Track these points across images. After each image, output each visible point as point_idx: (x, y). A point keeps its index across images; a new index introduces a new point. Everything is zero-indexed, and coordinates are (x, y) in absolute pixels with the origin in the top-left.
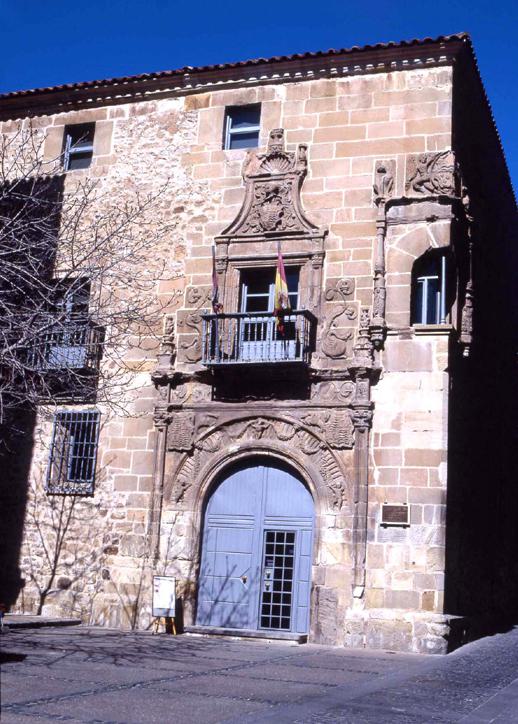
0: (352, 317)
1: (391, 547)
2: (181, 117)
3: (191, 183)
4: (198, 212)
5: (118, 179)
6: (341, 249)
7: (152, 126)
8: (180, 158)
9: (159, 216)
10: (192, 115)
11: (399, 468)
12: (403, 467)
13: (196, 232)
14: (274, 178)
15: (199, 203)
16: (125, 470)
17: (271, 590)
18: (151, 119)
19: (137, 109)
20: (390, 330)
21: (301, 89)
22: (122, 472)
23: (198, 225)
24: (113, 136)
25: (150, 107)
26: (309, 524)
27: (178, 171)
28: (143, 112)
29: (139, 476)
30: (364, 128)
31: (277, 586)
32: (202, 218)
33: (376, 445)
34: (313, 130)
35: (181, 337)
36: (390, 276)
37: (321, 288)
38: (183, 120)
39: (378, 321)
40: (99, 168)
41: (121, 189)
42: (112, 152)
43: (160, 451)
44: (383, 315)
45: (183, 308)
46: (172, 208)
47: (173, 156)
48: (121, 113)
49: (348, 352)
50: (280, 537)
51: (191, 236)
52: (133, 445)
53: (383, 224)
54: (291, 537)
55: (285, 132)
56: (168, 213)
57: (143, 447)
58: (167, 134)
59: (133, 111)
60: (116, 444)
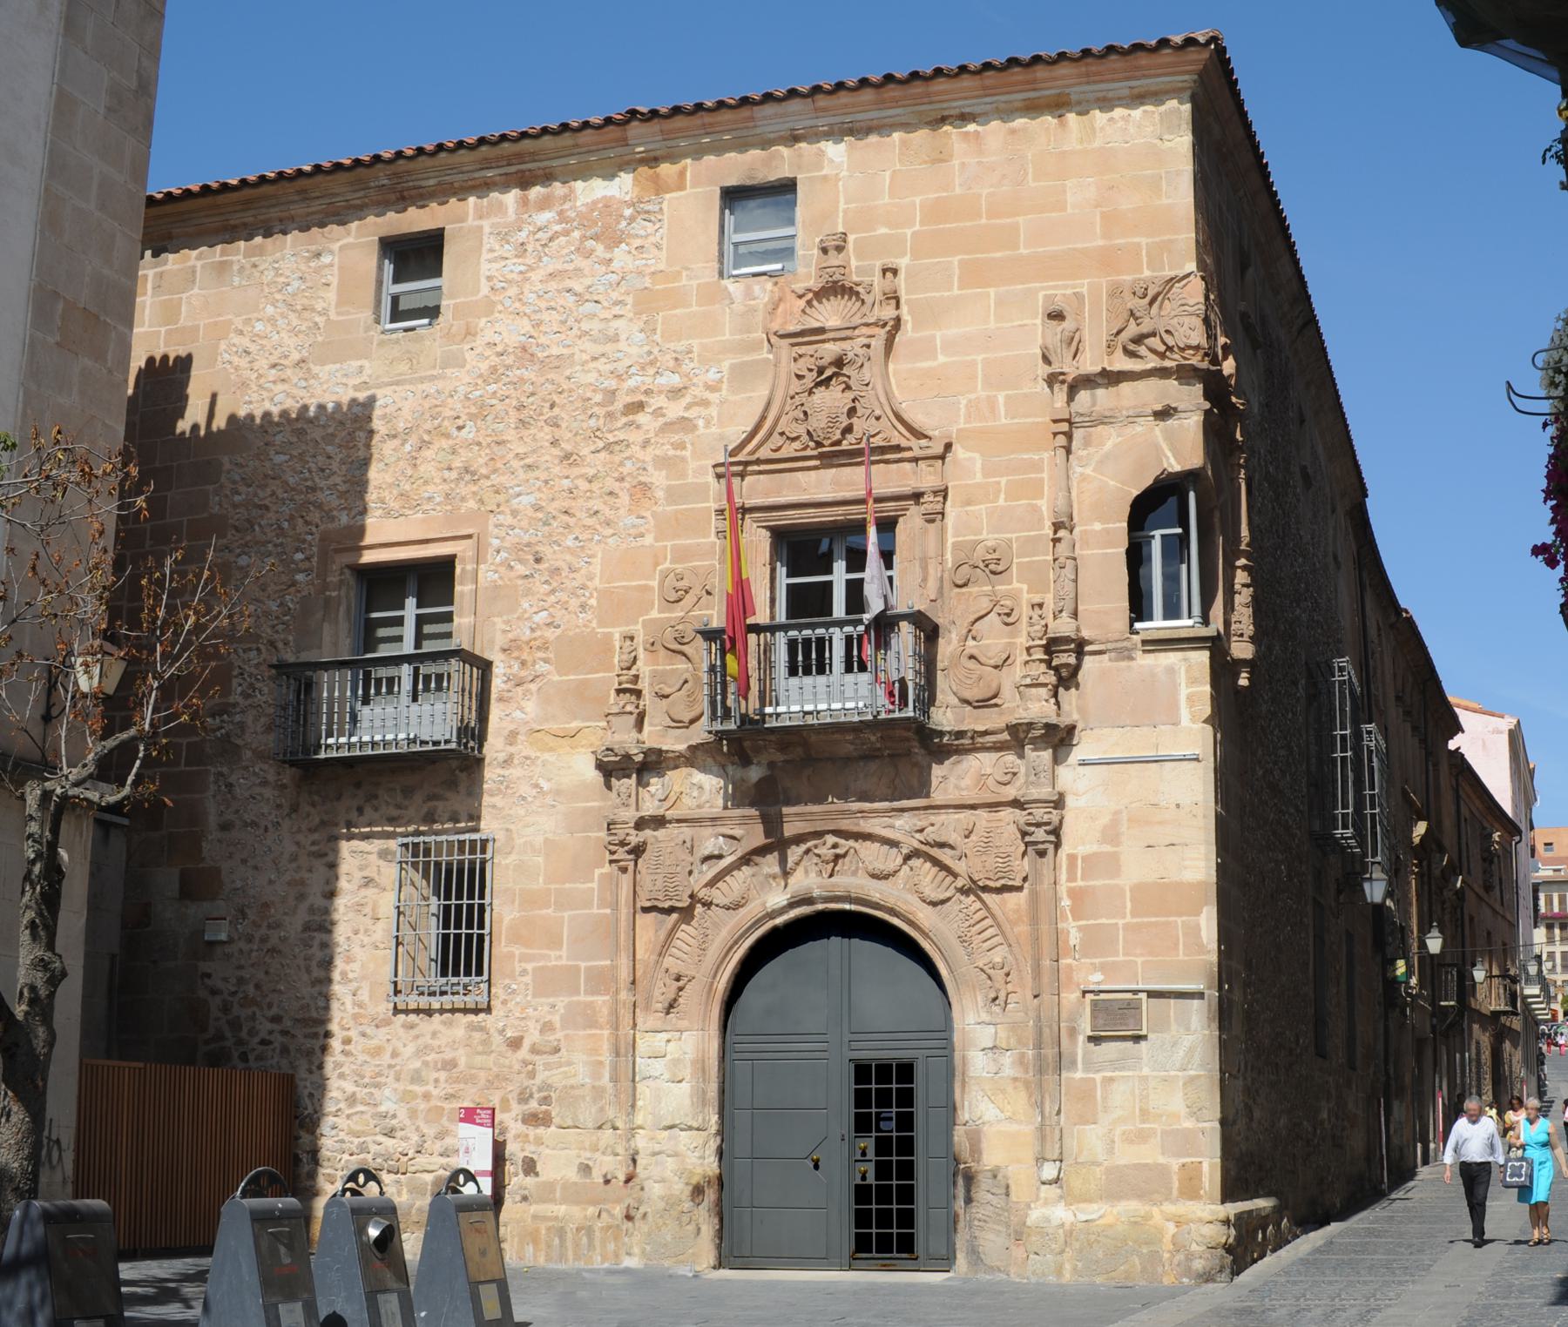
2: (628, 212)
4: (675, 410)
5: (499, 349)
6: (979, 478)
8: (630, 300)
9: (592, 422)
11: (1121, 922)
12: (1129, 919)
13: (671, 453)
15: (675, 393)
16: (552, 953)
17: (871, 1179)
18: (562, 218)
20: (1091, 643)
23: (676, 438)
24: (485, 256)
28: (544, 204)
29: (583, 965)
31: (882, 1170)
32: (685, 424)
34: (909, 232)
38: (632, 219)
41: (508, 367)
43: (625, 912)
45: (654, 614)
46: (618, 406)
47: (615, 295)
50: (884, 1070)
51: (663, 462)
56: (610, 415)
57: (587, 904)
58: (600, 249)
60: (531, 900)
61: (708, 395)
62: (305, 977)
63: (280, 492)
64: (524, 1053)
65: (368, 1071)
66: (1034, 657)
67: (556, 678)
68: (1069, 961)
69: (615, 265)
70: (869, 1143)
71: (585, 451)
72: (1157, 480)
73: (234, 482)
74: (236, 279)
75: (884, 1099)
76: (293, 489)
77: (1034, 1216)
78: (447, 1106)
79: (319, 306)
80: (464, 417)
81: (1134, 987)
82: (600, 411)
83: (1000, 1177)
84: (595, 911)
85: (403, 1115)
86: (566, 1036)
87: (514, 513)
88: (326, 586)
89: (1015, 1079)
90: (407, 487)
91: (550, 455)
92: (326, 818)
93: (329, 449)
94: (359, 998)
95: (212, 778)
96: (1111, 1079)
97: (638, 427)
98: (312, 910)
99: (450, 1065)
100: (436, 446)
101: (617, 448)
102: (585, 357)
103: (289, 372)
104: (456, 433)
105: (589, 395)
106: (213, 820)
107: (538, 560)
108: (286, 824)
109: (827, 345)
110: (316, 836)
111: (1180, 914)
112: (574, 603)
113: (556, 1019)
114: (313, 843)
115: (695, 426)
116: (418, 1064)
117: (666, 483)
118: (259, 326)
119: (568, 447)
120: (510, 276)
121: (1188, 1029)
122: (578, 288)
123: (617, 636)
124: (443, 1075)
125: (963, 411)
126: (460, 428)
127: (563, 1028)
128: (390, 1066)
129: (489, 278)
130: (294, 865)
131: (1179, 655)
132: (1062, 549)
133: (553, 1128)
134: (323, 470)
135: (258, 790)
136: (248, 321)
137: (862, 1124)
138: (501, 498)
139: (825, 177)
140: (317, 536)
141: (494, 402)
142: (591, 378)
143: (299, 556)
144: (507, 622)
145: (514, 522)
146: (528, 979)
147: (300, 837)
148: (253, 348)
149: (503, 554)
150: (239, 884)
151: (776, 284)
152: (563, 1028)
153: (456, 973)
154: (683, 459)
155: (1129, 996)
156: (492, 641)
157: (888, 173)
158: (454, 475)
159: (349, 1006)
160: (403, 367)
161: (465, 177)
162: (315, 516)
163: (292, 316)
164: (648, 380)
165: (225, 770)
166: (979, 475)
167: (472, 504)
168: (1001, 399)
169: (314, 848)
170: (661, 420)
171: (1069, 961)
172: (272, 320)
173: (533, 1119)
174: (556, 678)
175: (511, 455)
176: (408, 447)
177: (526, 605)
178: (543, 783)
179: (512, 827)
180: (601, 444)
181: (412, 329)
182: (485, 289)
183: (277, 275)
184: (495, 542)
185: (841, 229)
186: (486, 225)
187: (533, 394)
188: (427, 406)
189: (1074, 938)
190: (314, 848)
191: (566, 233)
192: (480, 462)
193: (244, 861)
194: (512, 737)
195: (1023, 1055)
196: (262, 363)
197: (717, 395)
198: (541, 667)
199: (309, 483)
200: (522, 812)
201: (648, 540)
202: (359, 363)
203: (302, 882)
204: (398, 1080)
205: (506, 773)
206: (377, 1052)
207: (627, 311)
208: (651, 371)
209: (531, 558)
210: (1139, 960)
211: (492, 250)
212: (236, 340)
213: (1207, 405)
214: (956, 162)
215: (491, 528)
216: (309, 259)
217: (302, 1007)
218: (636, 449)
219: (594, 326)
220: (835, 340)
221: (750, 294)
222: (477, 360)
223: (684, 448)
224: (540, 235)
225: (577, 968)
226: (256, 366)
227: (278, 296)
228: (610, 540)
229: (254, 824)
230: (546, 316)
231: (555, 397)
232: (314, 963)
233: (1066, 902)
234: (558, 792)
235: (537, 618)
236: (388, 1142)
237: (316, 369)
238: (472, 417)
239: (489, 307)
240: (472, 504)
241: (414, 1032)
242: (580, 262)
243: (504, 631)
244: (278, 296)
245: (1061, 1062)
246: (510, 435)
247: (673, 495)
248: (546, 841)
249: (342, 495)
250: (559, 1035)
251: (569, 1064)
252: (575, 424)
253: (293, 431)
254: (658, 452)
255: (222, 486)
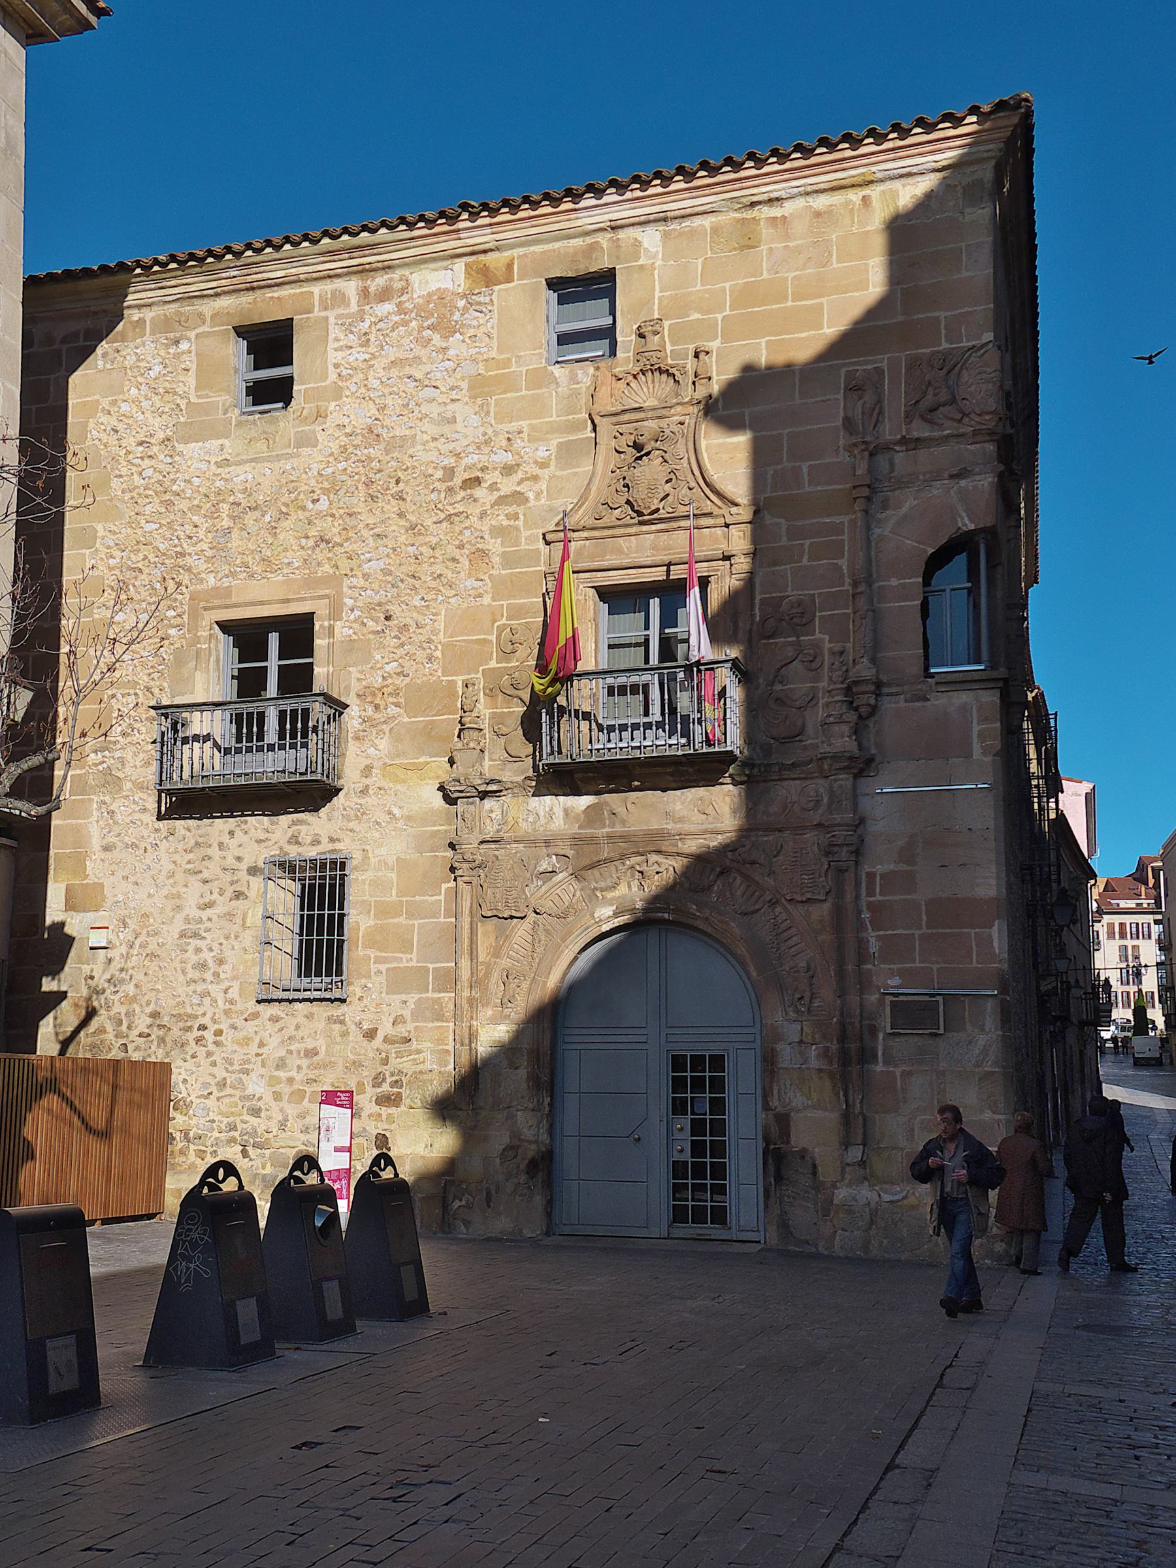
0: (814, 665)
1: (910, 1073)
2: (461, 303)
3: (490, 431)
4: (508, 486)
5: (348, 430)
6: (784, 541)
7: (405, 323)
8: (464, 385)
9: (434, 496)
10: (481, 299)
11: (917, 933)
12: (924, 930)
13: (505, 523)
14: (650, 414)
15: (508, 470)
16: (404, 956)
17: (687, 1156)
18: (401, 310)
19: (372, 290)
20: (889, 685)
21: (693, 232)
22: (395, 959)
23: (511, 510)
24: (332, 345)
25: (398, 285)
26: (674, 1038)
27: (464, 412)
28: (384, 295)
29: (431, 966)
30: (819, 309)
31: (697, 1148)
32: (518, 498)
33: (871, 893)
34: (719, 317)
35: (493, 716)
36: (879, 587)
37: (753, 616)
38: (465, 310)
39: (865, 670)
40: (310, 408)
41: (356, 447)
42: (332, 376)
43: (466, 920)
44: (873, 660)
45: (493, 664)
46: (457, 481)
47: (451, 381)
48: (340, 299)
49: (810, 730)
50: (698, 1061)
51: (498, 531)
52: (414, 912)
53: (866, 492)
54: (718, 1062)
55: (666, 324)
56: (450, 490)
57: (435, 915)
58: (437, 339)
59: (365, 293)
60: (384, 911)
61: (539, 472)
62: (181, 978)
63: (152, 557)
64: (378, 1041)
65: (237, 1058)
66: (836, 699)
67: (406, 720)
68: (870, 966)
69: (452, 353)
70: (685, 1121)
71: (428, 522)
72: (951, 540)
73: (108, 547)
74: (100, 363)
75: (698, 1084)
76: (164, 554)
77: (842, 1194)
78: (308, 1089)
79: (180, 391)
80: (318, 492)
81: (932, 991)
82: (442, 486)
83: (807, 1158)
84: (442, 920)
85: (268, 1097)
86: (416, 1028)
87: (366, 576)
88: (197, 639)
89: (820, 1070)
90: (268, 553)
91: (396, 527)
92: (200, 840)
93: (195, 518)
94: (229, 996)
95: (95, 806)
96: (910, 1073)
97: (475, 500)
98: (187, 920)
99: (311, 1053)
100: (293, 518)
101: (457, 519)
102: (426, 437)
103: (155, 449)
104: (310, 506)
105: (430, 471)
106: (96, 843)
107: (387, 618)
108: (164, 845)
109: (645, 423)
110: (191, 856)
111: (973, 927)
112: (421, 655)
113: (407, 1013)
114: (189, 862)
115: (527, 500)
116: (283, 1053)
117: (501, 550)
118: (125, 407)
119: (413, 518)
120: (354, 365)
121: (982, 1030)
122: (418, 376)
123: (460, 683)
124: (305, 1062)
125: (769, 481)
126: (315, 501)
127: (413, 1021)
128: (257, 1055)
129: (336, 366)
130: (171, 881)
131: (971, 693)
132: (862, 602)
133: (403, 1108)
134: (190, 538)
135: (137, 816)
136: (114, 403)
137: (679, 1107)
138: (354, 563)
139: (641, 266)
140: (187, 596)
141: (344, 478)
142: (433, 456)
143: (171, 613)
144: (361, 672)
145: (367, 585)
146: (382, 978)
147: (177, 857)
148: (121, 427)
149: (357, 613)
150: (120, 898)
151: (597, 368)
152: (413, 1021)
153: (318, 974)
154: (517, 529)
155: (927, 998)
156: (347, 688)
157: (700, 261)
158: (311, 542)
159: (220, 1002)
160: (261, 446)
161: (310, 269)
162: (185, 578)
163: (156, 398)
164: (484, 458)
165: (107, 799)
166: (784, 538)
167: (327, 568)
168: (805, 470)
169: (189, 866)
170: (496, 494)
171: (870, 966)
172: (136, 401)
173: (385, 1100)
174: (406, 720)
175: (361, 526)
176: (267, 518)
177: (378, 657)
178: (396, 811)
179: (368, 847)
180: (442, 516)
181: (269, 411)
182: (332, 376)
183: (138, 360)
184: (349, 602)
185: (656, 316)
186: (331, 315)
187: (380, 471)
188: (284, 481)
189: (874, 946)
190: (189, 866)
191: (405, 323)
192: (333, 530)
193: (126, 878)
194: (367, 771)
195: (827, 1049)
196: (130, 442)
197: (546, 471)
198: (392, 710)
199: (179, 549)
200: (377, 835)
201: (487, 600)
202: (220, 442)
203: (179, 896)
204: (263, 1066)
205: (363, 801)
206: (247, 1041)
207: (464, 395)
208: (486, 450)
209: (382, 617)
210: (935, 967)
211: (337, 340)
212: (104, 419)
213: (1002, 468)
214: (764, 248)
215: (345, 589)
216: (167, 346)
217: (178, 1004)
218: (474, 519)
219: (434, 410)
220: (652, 418)
221: (578, 377)
222: (328, 440)
223: (517, 519)
224: (381, 325)
225: (427, 969)
226: (124, 443)
227: (140, 379)
228: (453, 600)
229: (134, 846)
230: (389, 401)
231: (400, 474)
232: (189, 966)
233: (866, 915)
234: (409, 818)
235: (388, 668)
236: (254, 1121)
237: (180, 447)
238: (326, 491)
239: (337, 393)
240: (327, 568)
241: (278, 1025)
242: (423, 353)
243: (358, 679)
244: (140, 379)
245: (866, 1056)
246: (361, 508)
247: (508, 560)
248: (398, 859)
249: (209, 559)
250: (410, 1026)
251: (419, 1052)
252: (418, 498)
253: (161, 502)
254: (493, 522)
255: (97, 550)
